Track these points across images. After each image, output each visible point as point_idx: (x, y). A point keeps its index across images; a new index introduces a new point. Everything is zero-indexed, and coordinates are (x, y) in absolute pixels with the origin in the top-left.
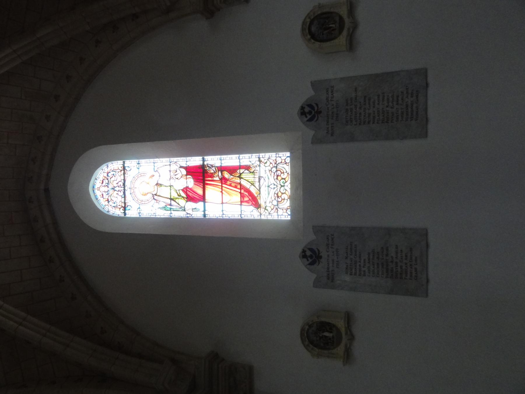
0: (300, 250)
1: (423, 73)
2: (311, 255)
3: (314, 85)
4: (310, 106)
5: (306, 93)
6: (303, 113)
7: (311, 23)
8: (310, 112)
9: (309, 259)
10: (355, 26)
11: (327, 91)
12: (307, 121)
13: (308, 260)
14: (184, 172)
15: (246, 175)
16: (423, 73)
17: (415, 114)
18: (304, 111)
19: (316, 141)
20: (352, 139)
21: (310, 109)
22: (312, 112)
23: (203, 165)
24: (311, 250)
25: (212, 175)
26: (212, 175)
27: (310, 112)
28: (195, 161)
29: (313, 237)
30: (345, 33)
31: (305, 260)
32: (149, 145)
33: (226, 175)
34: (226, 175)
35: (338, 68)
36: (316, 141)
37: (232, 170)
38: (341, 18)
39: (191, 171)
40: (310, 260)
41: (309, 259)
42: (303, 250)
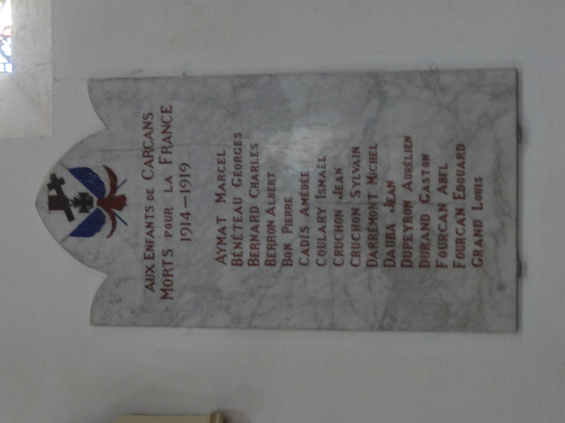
0: (43, 179)
2: (83, 195)
9: (75, 211)
11: (147, 125)
12: (76, 233)
13: (71, 218)
18: (60, 191)
21: (83, 189)
22: (91, 203)
24: (83, 174)
29: (89, 122)
31: (61, 215)
40: (80, 217)
41: (75, 211)
42: (53, 177)
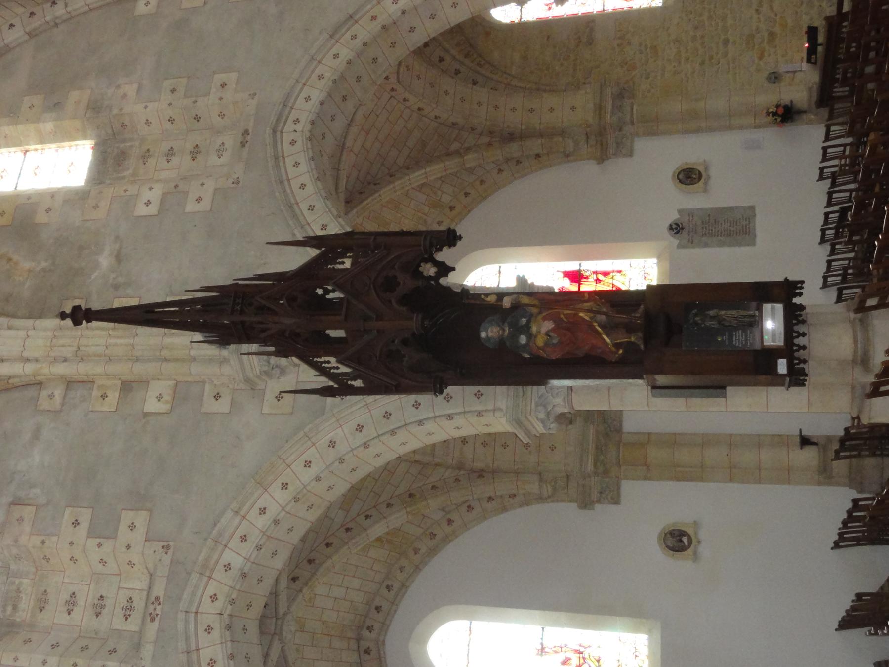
0: (667, 225)
1: (752, 208)
3: (680, 212)
4: (677, 224)
5: (674, 216)
6: (671, 228)
7: (679, 173)
8: (676, 228)
10: (709, 177)
14: (562, 275)
15: (618, 276)
16: (752, 208)
17: (283, 121)
19: (680, 246)
20: (706, 245)
23: (580, 270)
25: (587, 278)
26: (587, 278)
27: (676, 228)
28: (573, 266)
30: (702, 180)
32: (538, 248)
33: (600, 277)
34: (600, 277)
35: (696, 200)
36: (680, 246)
37: (606, 274)
38: (700, 173)
39: (567, 274)
